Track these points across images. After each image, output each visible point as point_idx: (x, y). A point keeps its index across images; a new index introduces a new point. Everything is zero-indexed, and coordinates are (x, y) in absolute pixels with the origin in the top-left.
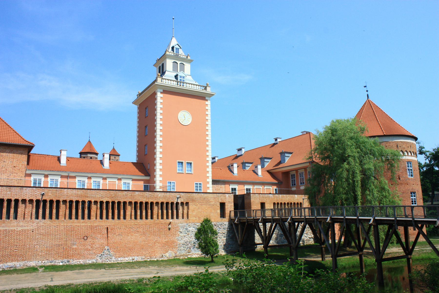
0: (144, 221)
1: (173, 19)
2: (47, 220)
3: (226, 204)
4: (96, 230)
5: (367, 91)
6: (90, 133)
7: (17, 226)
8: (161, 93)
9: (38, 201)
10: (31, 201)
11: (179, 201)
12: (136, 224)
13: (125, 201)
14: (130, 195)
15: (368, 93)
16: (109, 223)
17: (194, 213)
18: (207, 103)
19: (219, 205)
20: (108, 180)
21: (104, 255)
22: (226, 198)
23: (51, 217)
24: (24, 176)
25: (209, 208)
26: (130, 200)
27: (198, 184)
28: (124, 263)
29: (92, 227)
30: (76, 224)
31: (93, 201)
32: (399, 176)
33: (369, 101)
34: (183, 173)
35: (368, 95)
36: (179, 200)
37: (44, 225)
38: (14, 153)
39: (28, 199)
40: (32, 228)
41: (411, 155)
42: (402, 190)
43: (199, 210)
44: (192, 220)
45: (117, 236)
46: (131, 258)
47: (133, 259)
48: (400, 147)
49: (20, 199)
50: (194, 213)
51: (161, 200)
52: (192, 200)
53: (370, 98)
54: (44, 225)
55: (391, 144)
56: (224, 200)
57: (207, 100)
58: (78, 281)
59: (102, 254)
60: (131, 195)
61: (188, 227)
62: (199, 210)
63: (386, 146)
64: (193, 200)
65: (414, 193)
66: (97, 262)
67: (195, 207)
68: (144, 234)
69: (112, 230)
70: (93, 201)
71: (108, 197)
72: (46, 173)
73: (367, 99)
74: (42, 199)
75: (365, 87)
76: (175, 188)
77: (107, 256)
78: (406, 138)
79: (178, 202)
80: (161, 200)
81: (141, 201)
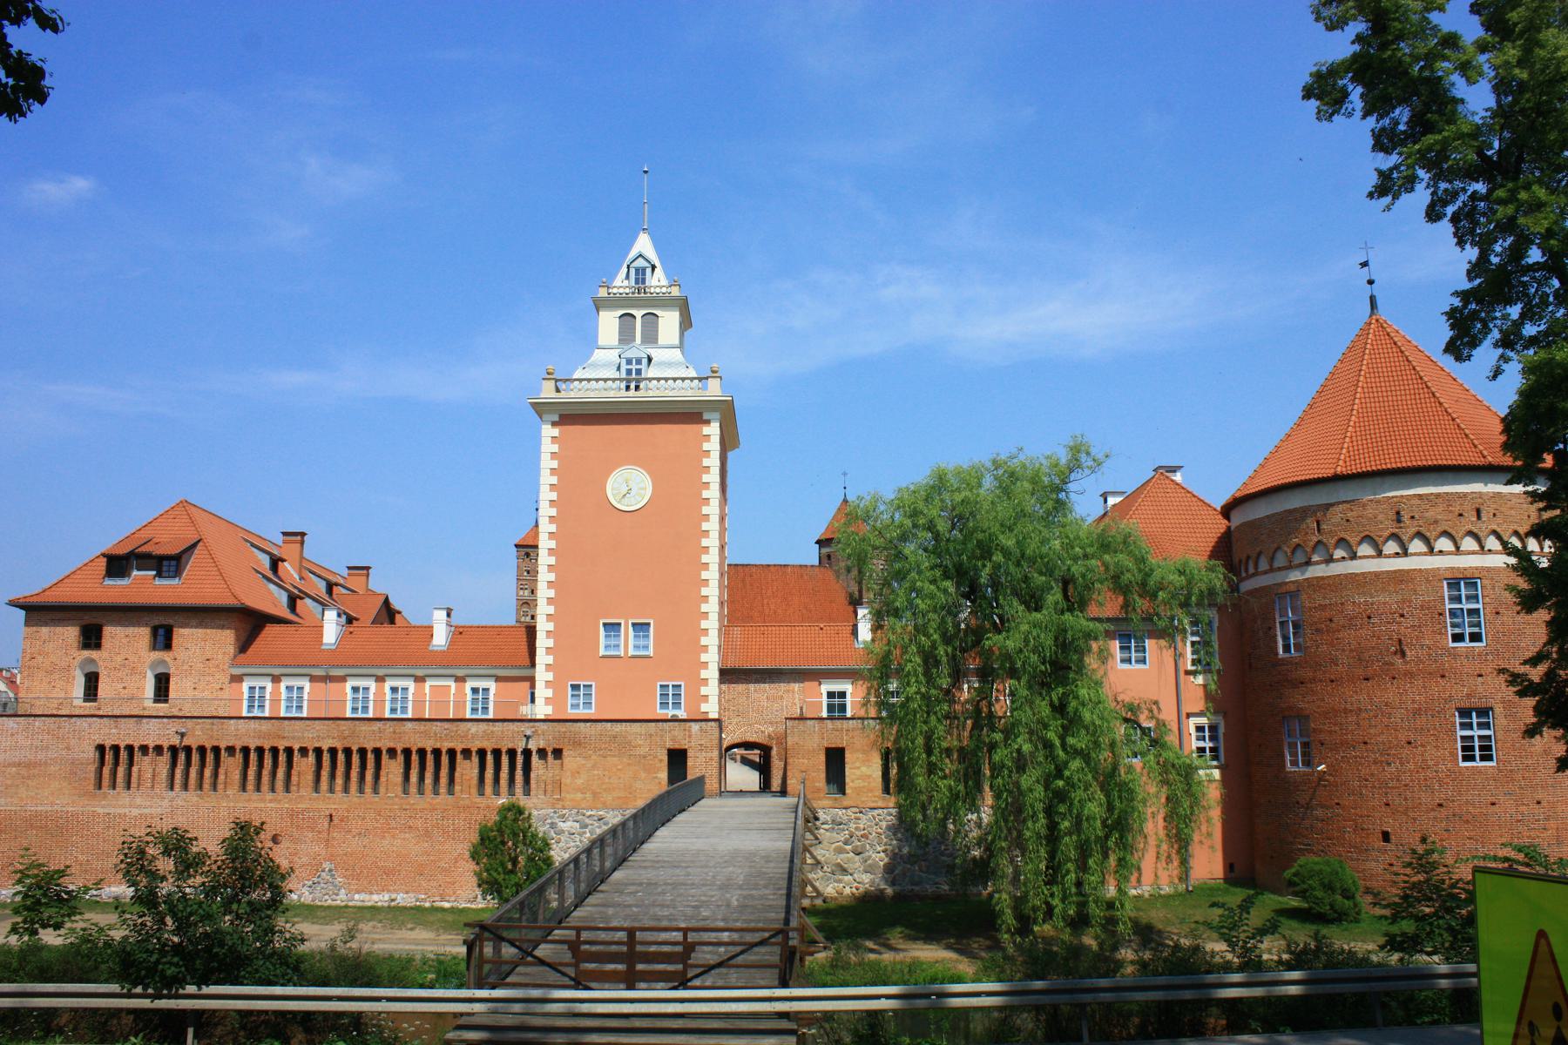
0: (428, 800)
1: (646, 172)
2: (192, 796)
3: (690, 754)
4: (303, 819)
5: (1371, 282)
7: (131, 806)
8: (554, 424)
9: (174, 750)
10: (159, 749)
11: (533, 746)
12: (404, 807)
13: (378, 745)
14: (391, 730)
15: (1376, 289)
16: (334, 804)
17: (579, 781)
18: (706, 430)
19: (665, 758)
21: (319, 883)
22: (690, 736)
23: (185, 787)
24: (227, 680)
25: (629, 764)
26: (392, 745)
28: (355, 907)
29: (292, 814)
30: (255, 805)
31: (296, 747)
32: (1400, 640)
33: (1381, 326)
35: (1373, 299)
36: (531, 742)
37: (184, 804)
38: (206, 627)
39: (151, 745)
40: (159, 810)
41: (1482, 550)
42: (1414, 701)
43: (596, 772)
44: (572, 800)
45: (354, 837)
46: (387, 898)
47: (393, 900)
48: (1413, 517)
49: (136, 745)
50: (579, 781)
51: (477, 742)
52: (574, 742)
53: (1383, 313)
54: (184, 804)
55: (1369, 512)
56: (683, 742)
57: (708, 422)
58: (386, 946)
59: (316, 880)
60: (394, 732)
61: (557, 820)
62: (596, 772)
63: (1348, 521)
66: (299, 901)
67: (583, 762)
68: (427, 834)
69: (342, 821)
70: (296, 747)
71: (333, 738)
72: (277, 671)
73: (1371, 316)
74: (181, 742)
75: (1365, 264)
76: (593, 701)
77: (325, 886)
78: (1450, 476)
79: (529, 747)
80: (477, 742)
81: (420, 745)
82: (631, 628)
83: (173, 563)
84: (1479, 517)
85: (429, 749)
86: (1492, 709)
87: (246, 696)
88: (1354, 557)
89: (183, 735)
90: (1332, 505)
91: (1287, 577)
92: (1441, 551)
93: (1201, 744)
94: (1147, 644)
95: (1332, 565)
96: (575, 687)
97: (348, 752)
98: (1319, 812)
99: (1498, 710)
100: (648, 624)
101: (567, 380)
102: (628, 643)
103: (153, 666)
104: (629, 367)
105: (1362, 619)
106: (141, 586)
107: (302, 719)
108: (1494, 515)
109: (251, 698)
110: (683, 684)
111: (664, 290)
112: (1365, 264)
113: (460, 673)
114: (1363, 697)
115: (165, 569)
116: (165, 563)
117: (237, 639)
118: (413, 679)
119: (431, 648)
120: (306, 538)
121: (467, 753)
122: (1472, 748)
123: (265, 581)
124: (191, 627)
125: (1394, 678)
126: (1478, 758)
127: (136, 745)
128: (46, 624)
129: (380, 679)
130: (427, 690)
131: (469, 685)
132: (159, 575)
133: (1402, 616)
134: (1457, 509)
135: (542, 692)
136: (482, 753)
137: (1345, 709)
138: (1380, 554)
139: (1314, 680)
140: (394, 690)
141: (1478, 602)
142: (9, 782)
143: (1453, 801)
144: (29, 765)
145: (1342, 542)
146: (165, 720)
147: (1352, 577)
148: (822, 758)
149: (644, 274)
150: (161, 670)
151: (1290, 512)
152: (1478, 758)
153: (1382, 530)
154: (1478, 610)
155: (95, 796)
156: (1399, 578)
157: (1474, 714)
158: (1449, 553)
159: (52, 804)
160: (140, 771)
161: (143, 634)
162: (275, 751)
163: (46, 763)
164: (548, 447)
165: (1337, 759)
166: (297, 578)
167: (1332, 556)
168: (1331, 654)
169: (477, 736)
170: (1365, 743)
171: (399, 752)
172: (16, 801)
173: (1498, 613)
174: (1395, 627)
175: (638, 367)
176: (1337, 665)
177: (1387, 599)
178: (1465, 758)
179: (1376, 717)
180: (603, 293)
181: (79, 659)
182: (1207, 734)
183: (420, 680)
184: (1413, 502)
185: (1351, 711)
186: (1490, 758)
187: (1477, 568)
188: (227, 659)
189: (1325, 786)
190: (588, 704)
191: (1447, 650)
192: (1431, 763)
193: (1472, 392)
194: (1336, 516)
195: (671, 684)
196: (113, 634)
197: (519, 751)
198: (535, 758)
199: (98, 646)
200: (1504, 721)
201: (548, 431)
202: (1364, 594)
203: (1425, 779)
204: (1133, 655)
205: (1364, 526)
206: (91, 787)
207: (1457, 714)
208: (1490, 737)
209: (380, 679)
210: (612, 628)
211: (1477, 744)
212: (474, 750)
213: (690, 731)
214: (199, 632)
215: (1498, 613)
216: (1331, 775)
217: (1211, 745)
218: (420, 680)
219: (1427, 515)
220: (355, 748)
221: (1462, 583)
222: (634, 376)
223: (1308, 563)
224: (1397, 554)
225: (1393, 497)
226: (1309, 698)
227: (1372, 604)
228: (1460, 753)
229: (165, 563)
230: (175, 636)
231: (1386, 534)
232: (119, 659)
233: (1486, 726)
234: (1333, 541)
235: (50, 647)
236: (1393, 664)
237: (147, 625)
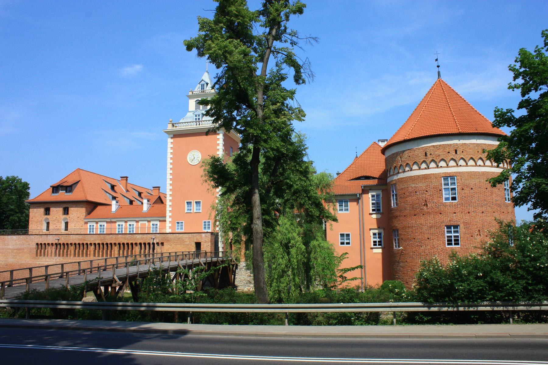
3: (202, 244)
5: (438, 66)
6: (356, 148)
8: (172, 138)
9: (56, 244)
10: (52, 244)
11: (155, 242)
18: (218, 137)
20: (140, 223)
22: (202, 238)
23: (59, 255)
24: (83, 224)
25: (184, 247)
26: (115, 242)
27: (206, 222)
31: (89, 243)
32: (426, 200)
34: (191, 213)
35: (439, 73)
36: (154, 240)
38: (78, 207)
39: (50, 243)
42: (430, 223)
48: (431, 154)
49: (46, 243)
53: (443, 78)
57: (219, 134)
60: (116, 238)
64: (168, 241)
65: (456, 227)
70: (89, 243)
72: (97, 220)
78: (445, 138)
81: (123, 242)
82: (195, 203)
83: (70, 188)
84: (456, 153)
85: (125, 243)
86: (459, 225)
87: (89, 228)
88: (411, 170)
89: (58, 240)
90: (405, 151)
91: (393, 178)
92: (441, 167)
93: (375, 240)
94: (349, 204)
95: (405, 173)
96: (178, 223)
97: (103, 244)
98: (401, 264)
99: (462, 226)
100: (200, 202)
101: (178, 123)
102: (194, 207)
103: (64, 220)
104: (196, 118)
105: (414, 193)
106: (62, 195)
107: (94, 234)
108: (463, 152)
109: (90, 229)
110: (183, 222)
111: (210, 91)
112: (437, 60)
113: (149, 219)
114: (414, 222)
115: (68, 190)
116: (68, 188)
117: (87, 211)
118: (95, 222)
119: (142, 212)
120: (128, 178)
121: (136, 244)
122: (451, 240)
123: (106, 193)
124: (74, 207)
125: (424, 215)
126: (453, 244)
127: (46, 243)
128: (35, 208)
129: (126, 222)
130: (139, 225)
131: (152, 223)
132: (66, 192)
133: (427, 191)
134: (447, 150)
135: (168, 224)
136: (140, 244)
137: (408, 226)
138: (420, 169)
139: (400, 216)
140: (130, 225)
141: (455, 185)
142: (15, 254)
143: (443, 260)
144: (19, 249)
145: (407, 164)
146: (54, 236)
147: (411, 177)
148: (194, 245)
149: (204, 86)
150: (66, 221)
151: (393, 154)
152: (453, 244)
153: (420, 159)
154: (455, 188)
155: (36, 258)
156: (426, 177)
157: (452, 228)
158: (444, 167)
159: (25, 261)
160: (135, 251)
161: (60, 210)
162: (83, 244)
163: (24, 249)
164: (170, 145)
165: (406, 245)
166: (125, 191)
167: (405, 170)
168: (404, 206)
169: (139, 239)
170: (414, 239)
171: (117, 244)
172: (16, 260)
173: (463, 189)
174: (424, 196)
175: (199, 117)
176: (406, 210)
177: (421, 185)
178: (448, 244)
179: (418, 229)
180: (190, 93)
181: (44, 218)
182: (377, 236)
183: (137, 222)
184: (431, 148)
185: (410, 227)
186: (458, 244)
187: (455, 172)
188: (84, 217)
189: (403, 255)
190: (182, 228)
191: (443, 203)
192: (436, 246)
193: (471, 105)
194: (406, 154)
195: (207, 221)
196: (53, 210)
197: (151, 243)
198: (156, 245)
199: (49, 214)
200: (464, 230)
201: (170, 140)
202: (414, 183)
203: (434, 252)
204: (344, 208)
205: (414, 158)
206: (35, 256)
207: (446, 228)
208: (458, 236)
209: (126, 222)
210: (189, 203)
211: (453, 239)
212: (138, 243)
213: (202, 236)
214: (76, 209)
215: (463, 189)
216: (404, 250)
217: (379, 240)
218: (137, 222)
219: (436, 153)
220: (105, 243)
221: (449, 178)
222: (197, 120)
223: (398, 173)
224: (426, 168)
225: (424, 147)
226: (399, 222)
227: (417, 187)
228: (446, 242)
229: (68, 188)
230: (69, 210)
231: (422, 161)
232: (55, 218)
233: (457, 232)
234: (405, 164)
235: (36, 215)
236: (423, 209)
237: (62, 207)
